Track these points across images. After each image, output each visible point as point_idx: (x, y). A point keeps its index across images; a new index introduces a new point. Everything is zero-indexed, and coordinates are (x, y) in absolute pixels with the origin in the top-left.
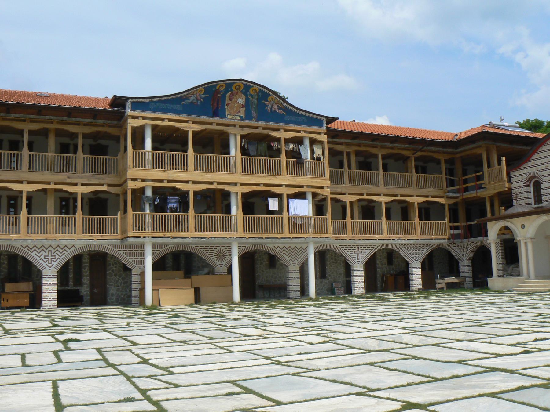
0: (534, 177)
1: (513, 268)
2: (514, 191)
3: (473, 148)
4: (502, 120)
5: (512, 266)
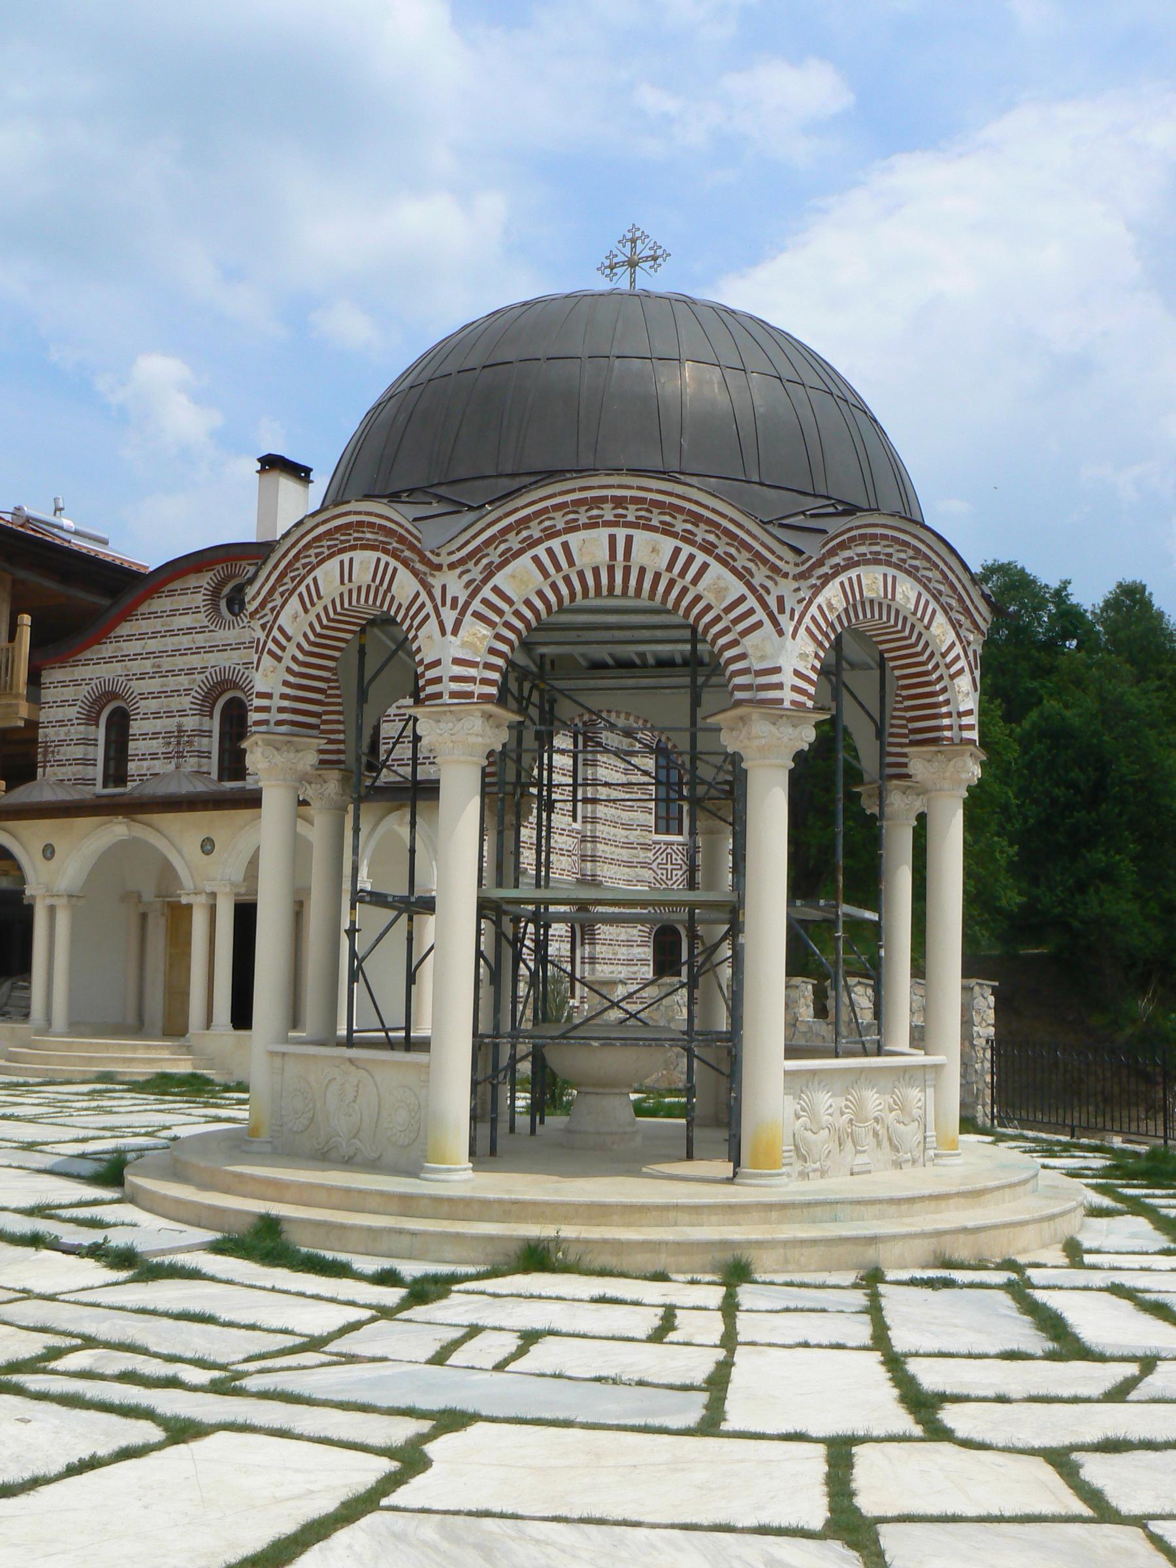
0: (111, 695)
1: (12, 988)
4: (58, 509)
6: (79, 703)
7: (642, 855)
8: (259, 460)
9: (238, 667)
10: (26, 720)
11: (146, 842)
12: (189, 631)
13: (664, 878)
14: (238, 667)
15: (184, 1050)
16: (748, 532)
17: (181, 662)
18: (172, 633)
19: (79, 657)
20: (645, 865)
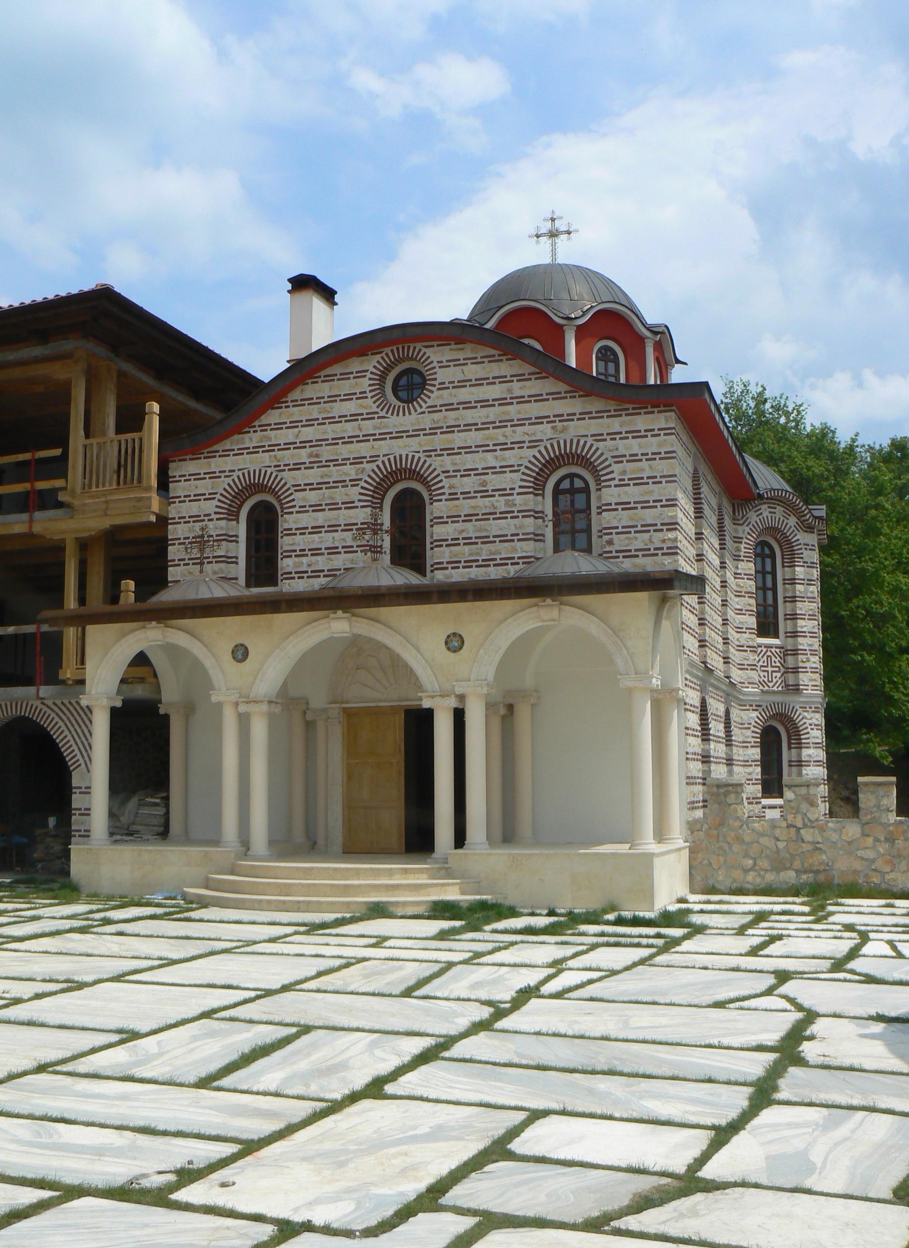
2: (176, 531)
3: (37, 361)
5: (134, 800)
6: (218, 496)
7: (752, 658)
8: (289, 280)
9: (269, 470)
10: (157, 515)
11: (370, 640)
13: (766, 680)
14: (417, 455)
15: (443, 872)
17: (344, 451)
18: (332, 420)
19: (215, 448)
20: (753, 667)
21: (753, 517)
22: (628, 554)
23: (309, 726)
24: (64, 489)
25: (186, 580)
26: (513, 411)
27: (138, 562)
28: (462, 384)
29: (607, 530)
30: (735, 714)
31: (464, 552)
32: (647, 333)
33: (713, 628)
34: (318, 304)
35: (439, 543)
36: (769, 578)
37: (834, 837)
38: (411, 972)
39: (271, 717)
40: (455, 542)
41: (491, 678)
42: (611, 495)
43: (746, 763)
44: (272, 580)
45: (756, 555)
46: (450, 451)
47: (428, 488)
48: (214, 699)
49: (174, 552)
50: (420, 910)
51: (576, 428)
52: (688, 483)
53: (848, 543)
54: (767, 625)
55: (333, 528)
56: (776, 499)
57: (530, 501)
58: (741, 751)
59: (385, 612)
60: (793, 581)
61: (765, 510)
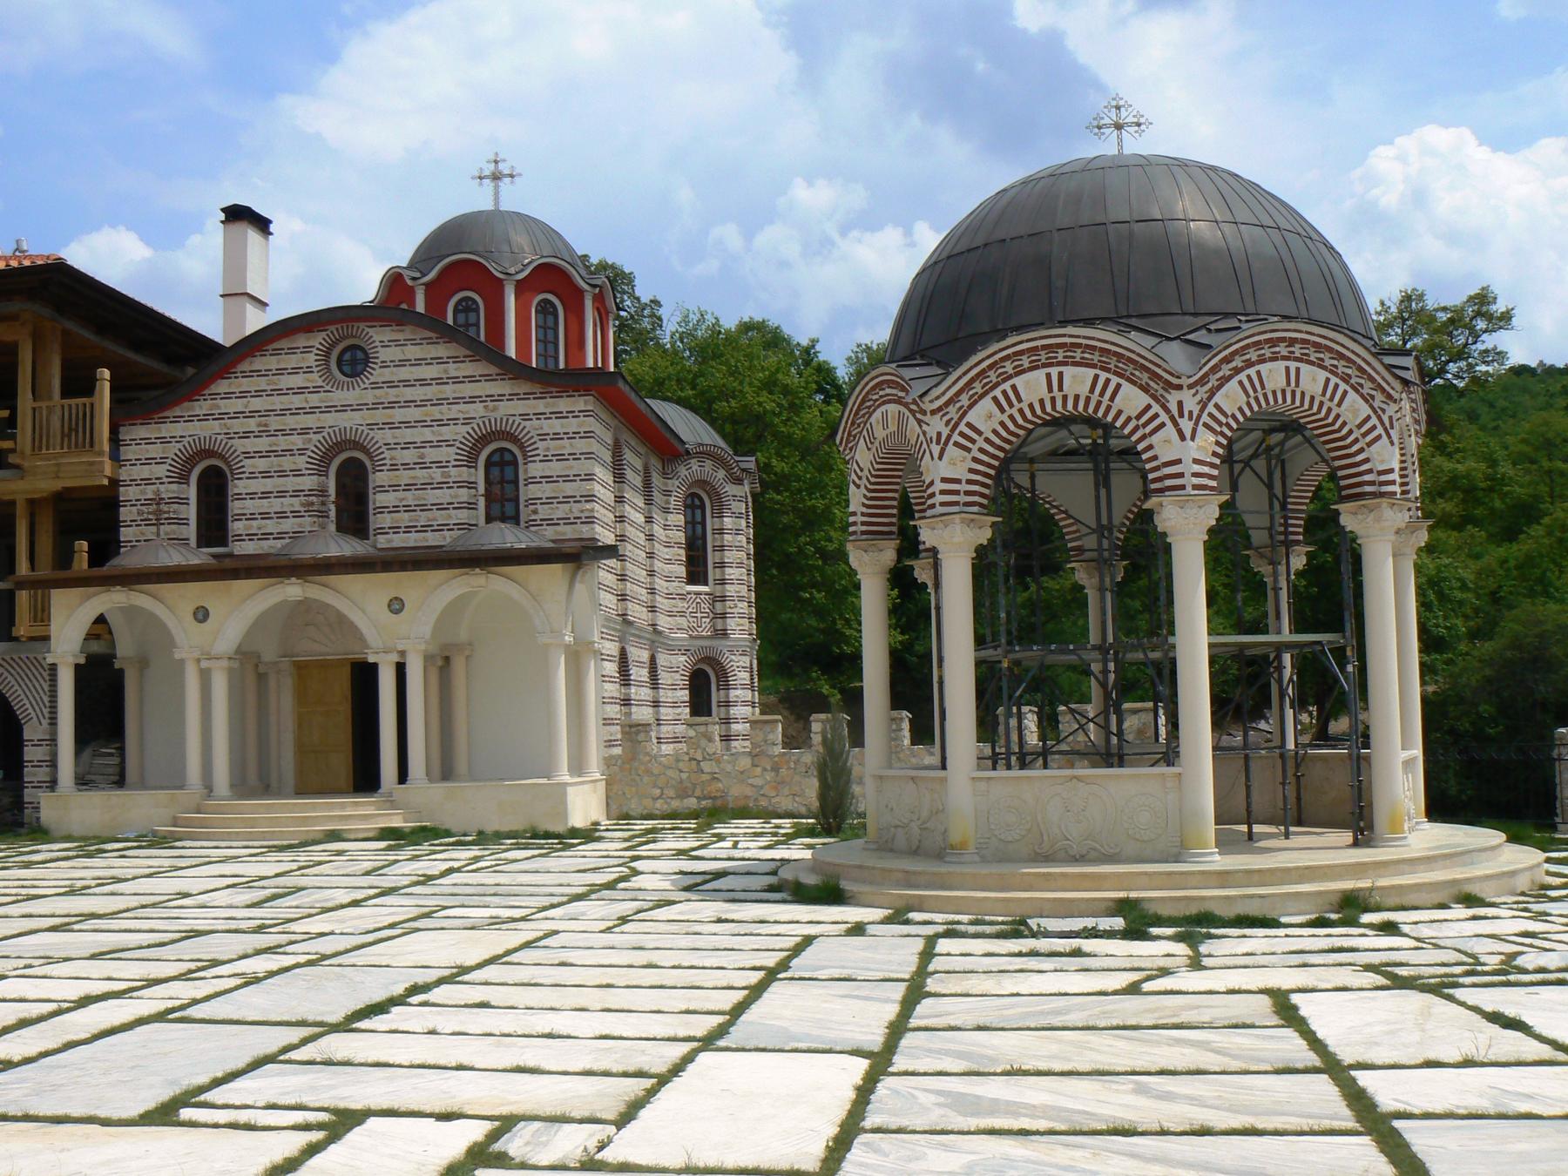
2: (127, 493)
7: (682, 605)
8: (223, 210)
12: (300, 391)
16: (1374, 369)
17: (291, 422)
18: (280, 392)
20: (682, 614)
21: (683, 471)
22: (551, 522)
23: (261, 678)
24: (13, 451)
25: (141, 541)
26: (449, 390)
27: (89, 528)
28: (402, 363)
29: (532, 501)
30: (663, 659)
31: (404, 518)
32: (586, 287)
33: (636, 582)
34: (253, 236)
35: (381, 510)
36: (699, 528)
37: (729, 768)
38: (368, 865)
39: (230, 671)
40: (395, 510)
41: (428, 636)
42: (536, 469)
43: (675, 705)
44: (223, 542)
45: (686, 506)
46: (391, 425)
47: (371, 458)
48: (177, 656)
49: (126, 513)
50: (371, 835)
51: (506, 408)
52: (607, 456)
53: (798, 479)
54: (696, 571)
55: (282, 494)
56: (705, 454)
57: (465, 474)
58: (670, 693)
59: (332, 579)
60: (721, 531)
61: (694, 464)
